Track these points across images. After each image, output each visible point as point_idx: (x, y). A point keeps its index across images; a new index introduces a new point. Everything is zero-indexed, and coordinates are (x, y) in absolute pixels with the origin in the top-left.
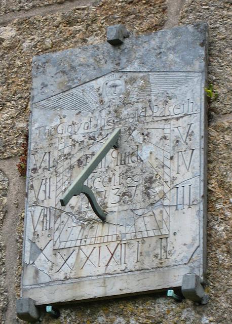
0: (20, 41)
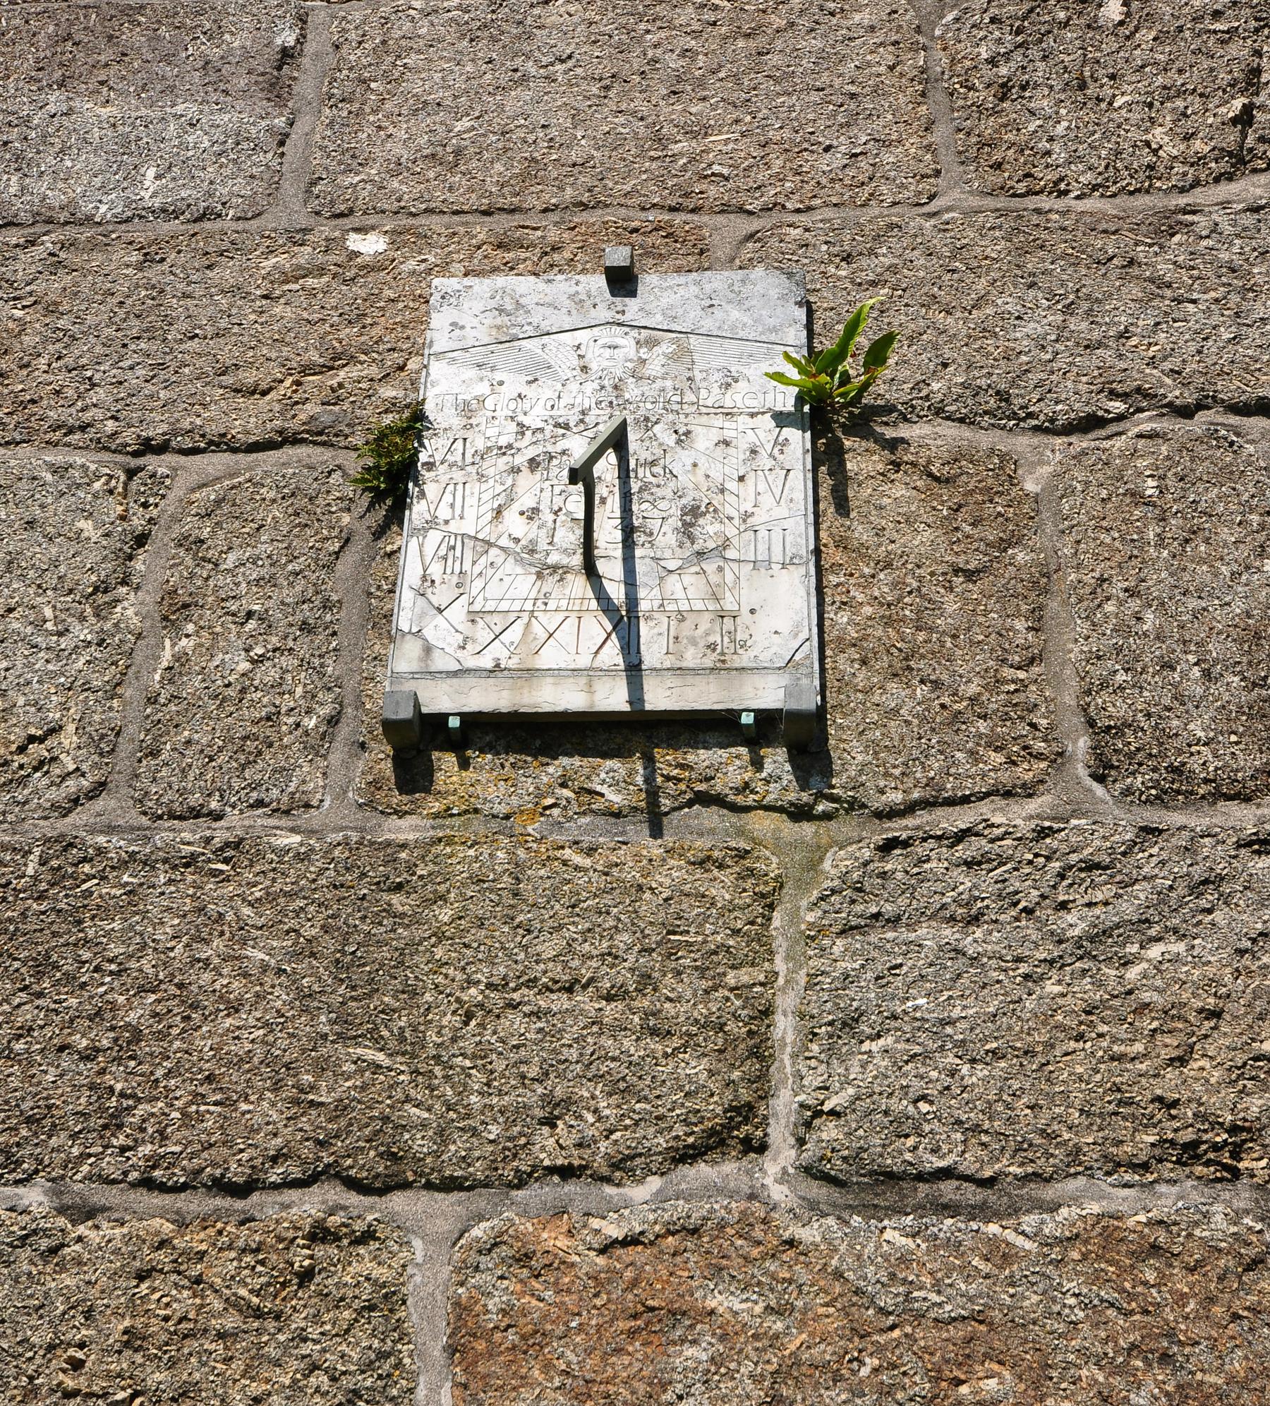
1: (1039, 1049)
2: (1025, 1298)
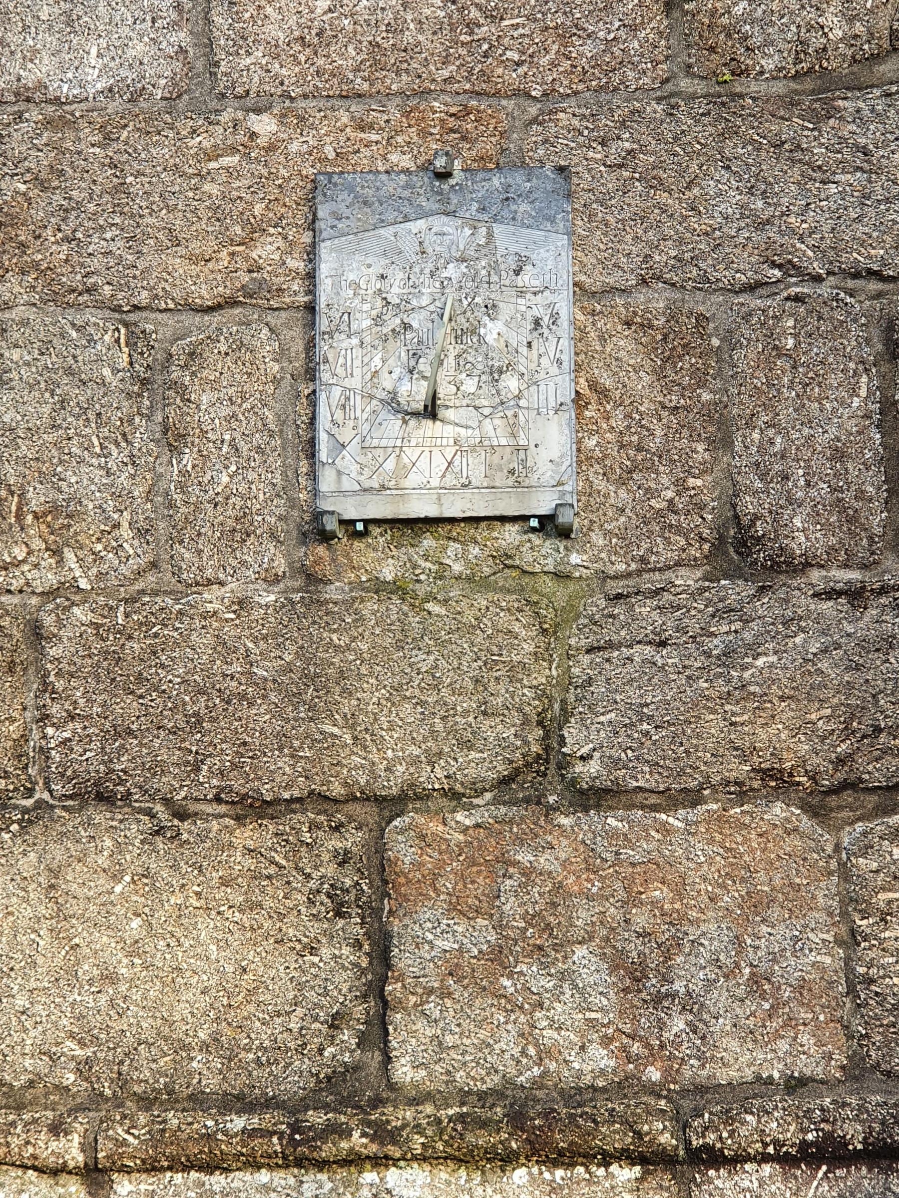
1: (693, 720)
2: (676, 851)
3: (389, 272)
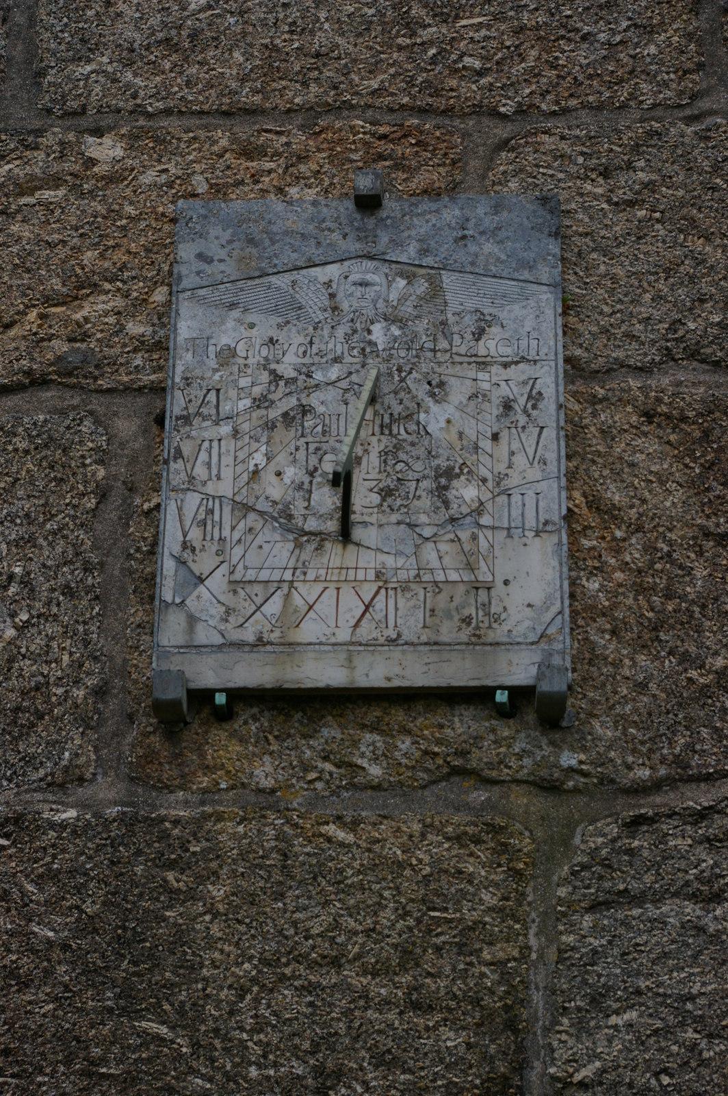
0: (133, 170)
3: (281, 336)
